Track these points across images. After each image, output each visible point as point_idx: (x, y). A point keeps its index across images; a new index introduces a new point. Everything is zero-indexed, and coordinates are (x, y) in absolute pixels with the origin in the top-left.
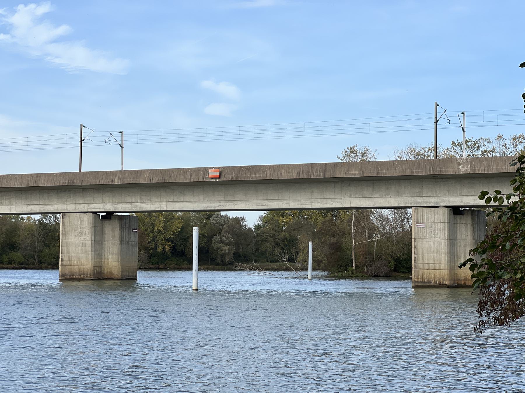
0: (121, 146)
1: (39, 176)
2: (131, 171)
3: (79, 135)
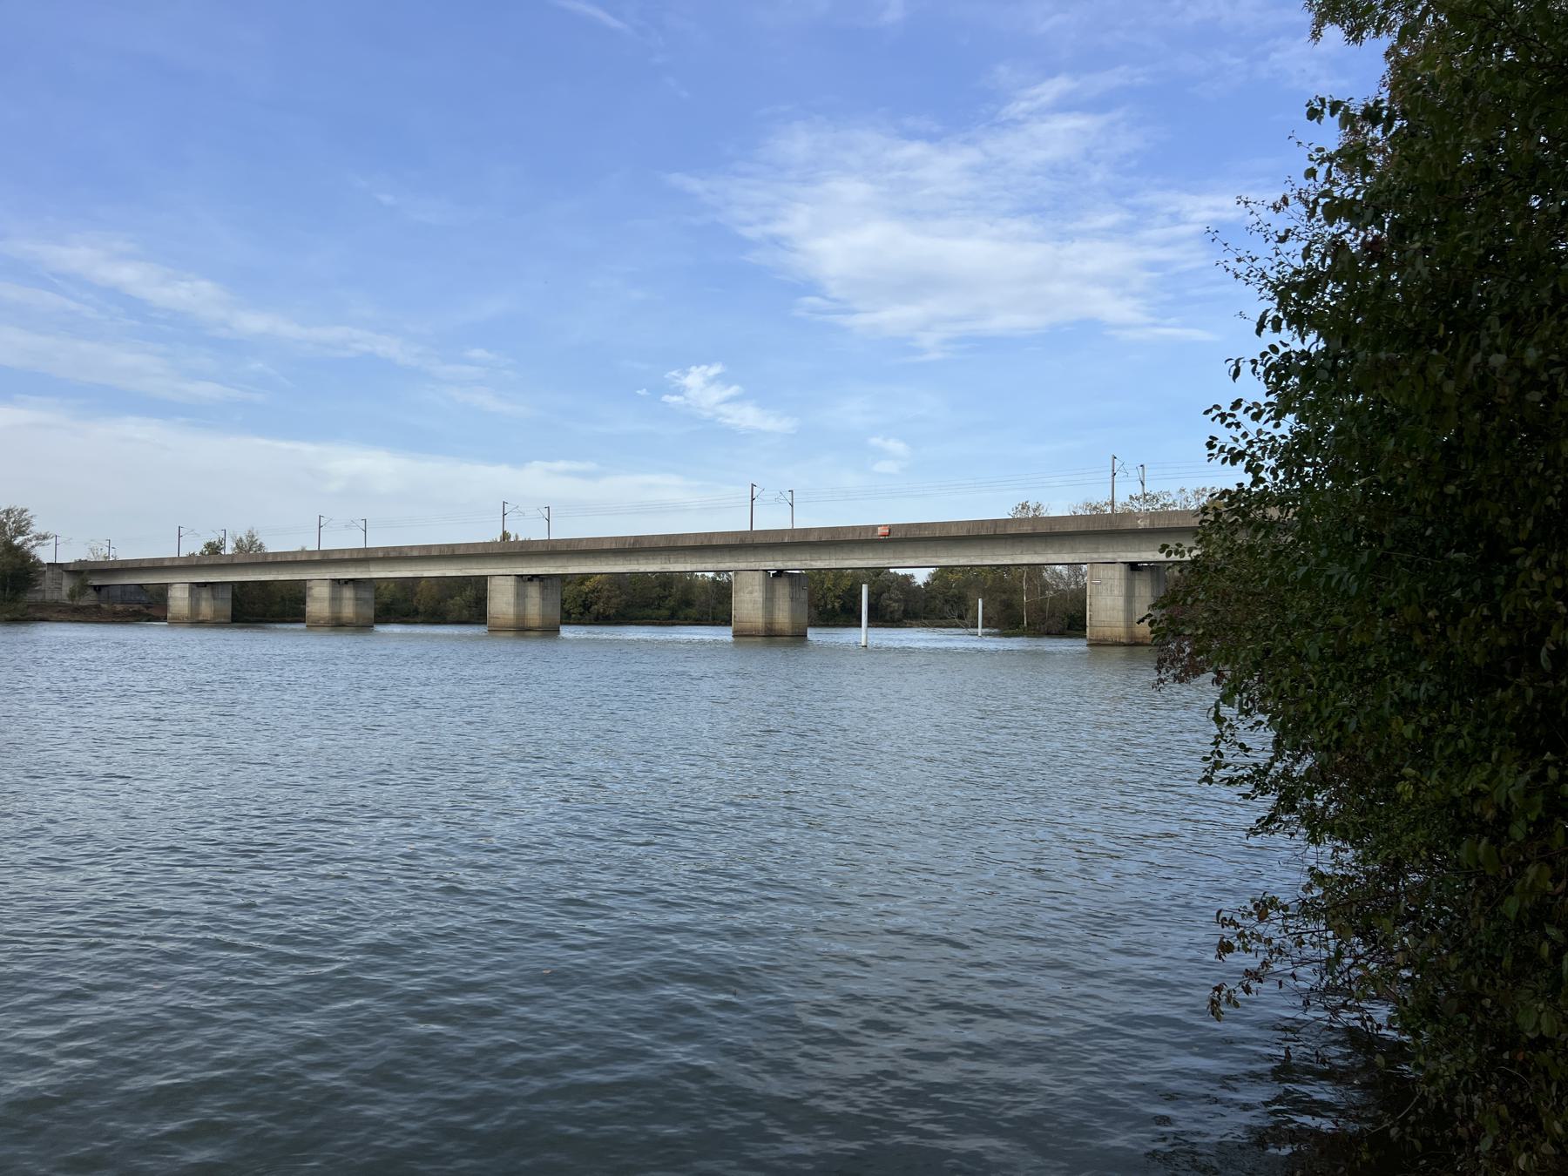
1: (162, 559)
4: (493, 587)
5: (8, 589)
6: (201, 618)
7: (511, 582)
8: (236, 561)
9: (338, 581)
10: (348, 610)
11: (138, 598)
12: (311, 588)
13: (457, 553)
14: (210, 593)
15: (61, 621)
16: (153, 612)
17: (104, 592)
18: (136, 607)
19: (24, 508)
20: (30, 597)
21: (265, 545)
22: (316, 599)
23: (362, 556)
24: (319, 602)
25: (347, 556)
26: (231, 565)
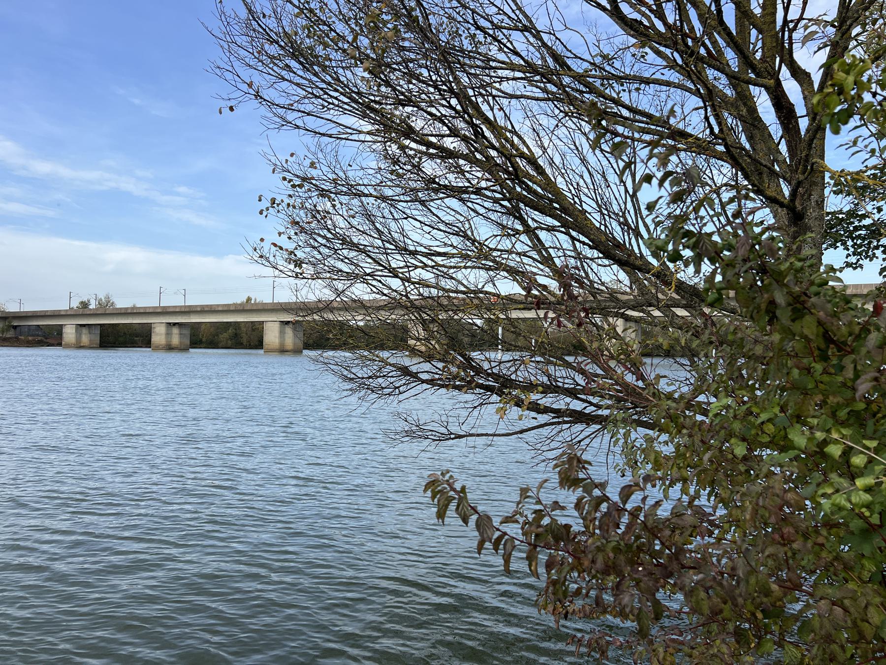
7: (277, 325)
10: (176, 340)
17: (18, 329)
18: (40, 338)
23: (187, 310)
24: (159, 335)
26: (94, 315)
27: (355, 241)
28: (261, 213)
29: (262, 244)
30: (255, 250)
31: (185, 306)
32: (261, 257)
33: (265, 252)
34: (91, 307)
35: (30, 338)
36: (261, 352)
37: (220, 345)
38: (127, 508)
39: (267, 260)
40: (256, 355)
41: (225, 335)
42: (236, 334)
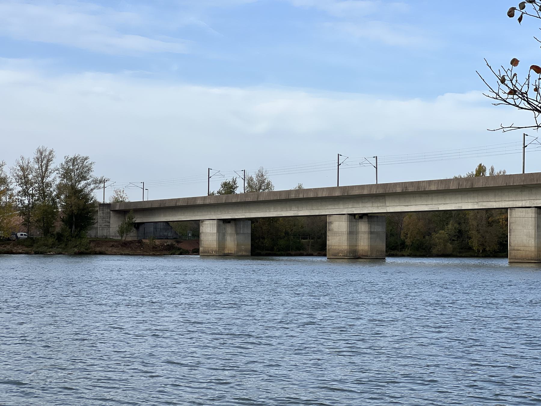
0: (375, 167)
1: (195, 199)
2: (381, 184)
3: (522, 143)
4: (513, 220)
5: (74, 227)
6: (226, 252)
8: (249, 199)
9: (354, 215)
11: (166, 234)
12: (331, 223)
13: (476, 186)
14: (234, 228)
15: (115, 254)
16: (183, 246)
17: (141, 228)
18: (169, 242)
19: (85, 156)
20: (91, 233)
21: (273, 183)
22: (335, 234)
23: (381, 191)
25: (366, 192)
26: (243, 204)
27: (501, 265)
28: (511, 14)
29: (515, 69)
30: (503, 81)
31: (377, 186)
32: (513, 92)
33: (520, 84)
34: (238, 191)
35: (158, 242)
36: (504, 262)
37: (434, 251)
38: (401, 384)
39: (524, 96)
40: (495, 268)
41: (443, 234)
42: (460, 231)
